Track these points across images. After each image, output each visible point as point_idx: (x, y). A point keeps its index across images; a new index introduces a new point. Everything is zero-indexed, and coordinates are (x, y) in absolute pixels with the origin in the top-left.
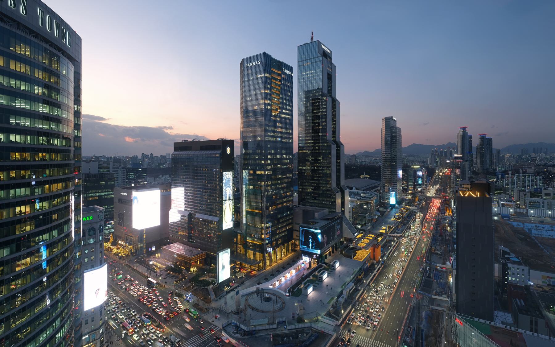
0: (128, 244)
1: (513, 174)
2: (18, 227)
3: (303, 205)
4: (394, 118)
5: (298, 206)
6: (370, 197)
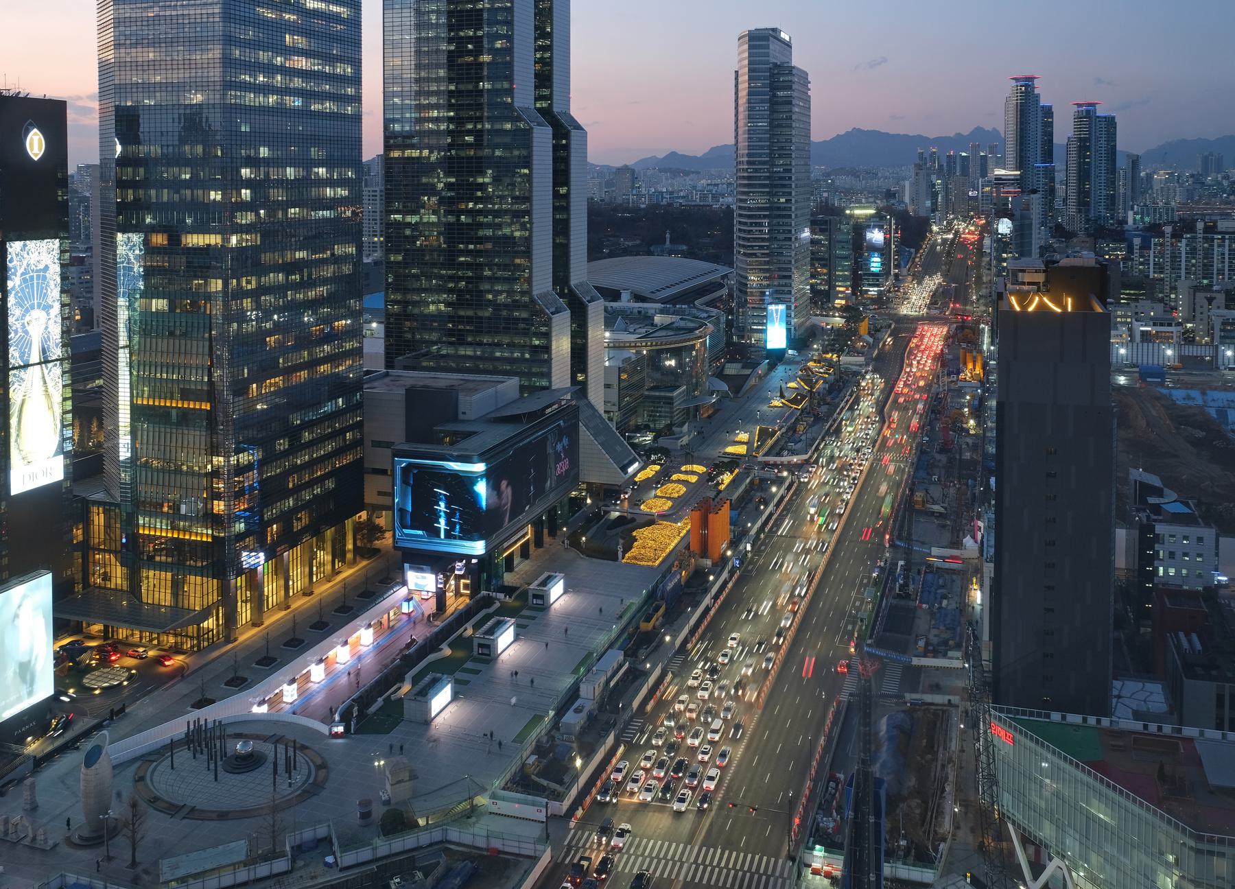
1: (1177, 235)
3: (406, 368)
5: (387, 375)
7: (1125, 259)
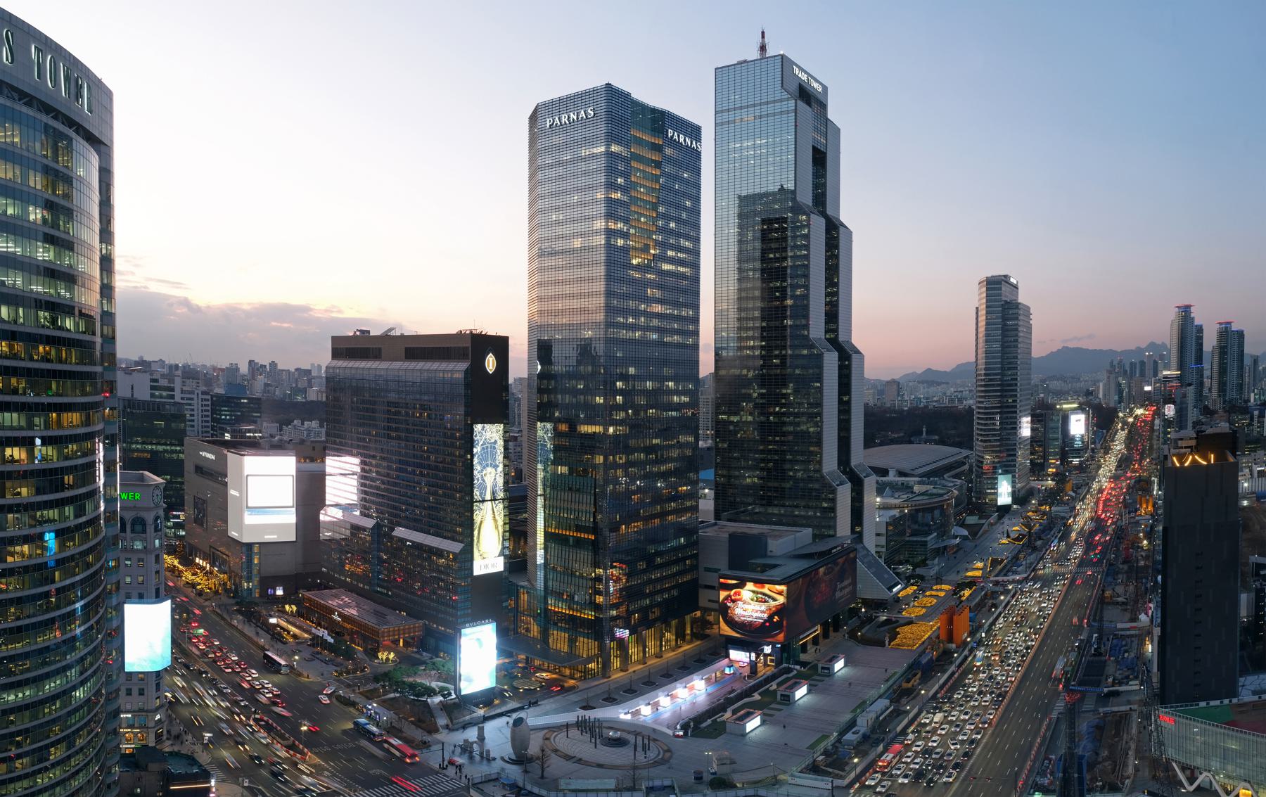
0: (216, 569)
2: (8, 484)
3: (729, 520)
4: (1013, 280)
5: (715, 524)
6: (942, 492)
7: (1250, 424)
